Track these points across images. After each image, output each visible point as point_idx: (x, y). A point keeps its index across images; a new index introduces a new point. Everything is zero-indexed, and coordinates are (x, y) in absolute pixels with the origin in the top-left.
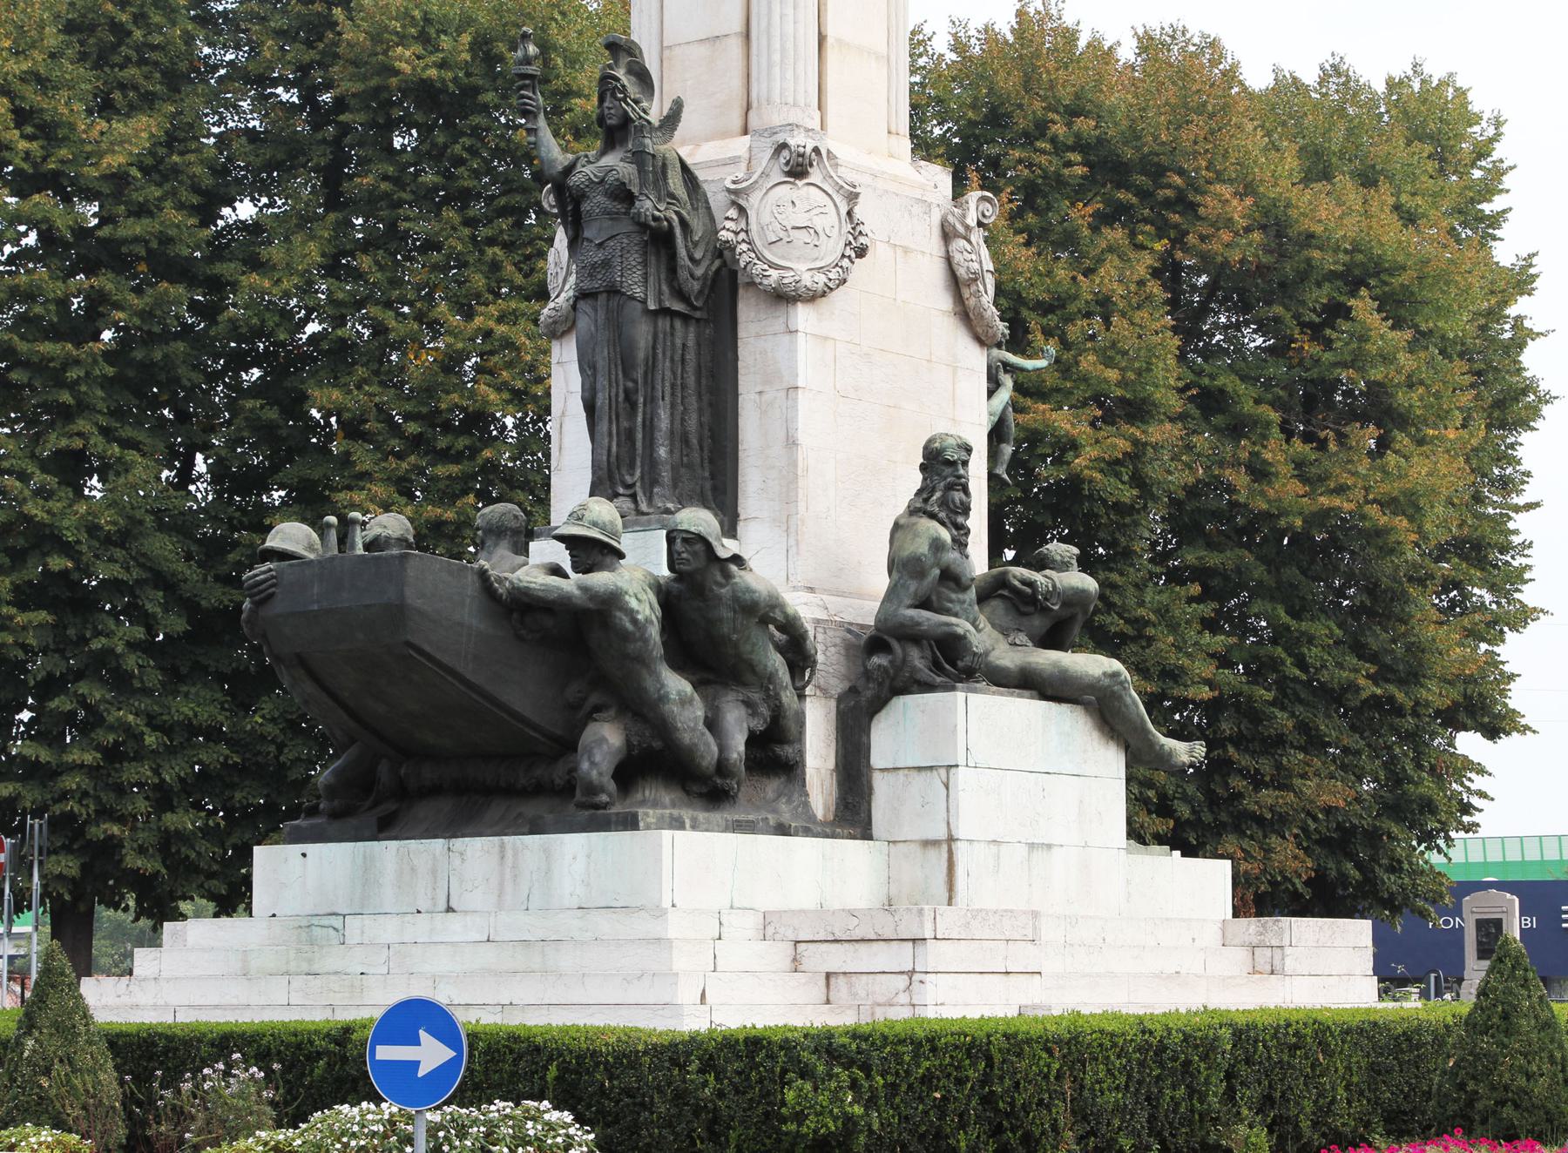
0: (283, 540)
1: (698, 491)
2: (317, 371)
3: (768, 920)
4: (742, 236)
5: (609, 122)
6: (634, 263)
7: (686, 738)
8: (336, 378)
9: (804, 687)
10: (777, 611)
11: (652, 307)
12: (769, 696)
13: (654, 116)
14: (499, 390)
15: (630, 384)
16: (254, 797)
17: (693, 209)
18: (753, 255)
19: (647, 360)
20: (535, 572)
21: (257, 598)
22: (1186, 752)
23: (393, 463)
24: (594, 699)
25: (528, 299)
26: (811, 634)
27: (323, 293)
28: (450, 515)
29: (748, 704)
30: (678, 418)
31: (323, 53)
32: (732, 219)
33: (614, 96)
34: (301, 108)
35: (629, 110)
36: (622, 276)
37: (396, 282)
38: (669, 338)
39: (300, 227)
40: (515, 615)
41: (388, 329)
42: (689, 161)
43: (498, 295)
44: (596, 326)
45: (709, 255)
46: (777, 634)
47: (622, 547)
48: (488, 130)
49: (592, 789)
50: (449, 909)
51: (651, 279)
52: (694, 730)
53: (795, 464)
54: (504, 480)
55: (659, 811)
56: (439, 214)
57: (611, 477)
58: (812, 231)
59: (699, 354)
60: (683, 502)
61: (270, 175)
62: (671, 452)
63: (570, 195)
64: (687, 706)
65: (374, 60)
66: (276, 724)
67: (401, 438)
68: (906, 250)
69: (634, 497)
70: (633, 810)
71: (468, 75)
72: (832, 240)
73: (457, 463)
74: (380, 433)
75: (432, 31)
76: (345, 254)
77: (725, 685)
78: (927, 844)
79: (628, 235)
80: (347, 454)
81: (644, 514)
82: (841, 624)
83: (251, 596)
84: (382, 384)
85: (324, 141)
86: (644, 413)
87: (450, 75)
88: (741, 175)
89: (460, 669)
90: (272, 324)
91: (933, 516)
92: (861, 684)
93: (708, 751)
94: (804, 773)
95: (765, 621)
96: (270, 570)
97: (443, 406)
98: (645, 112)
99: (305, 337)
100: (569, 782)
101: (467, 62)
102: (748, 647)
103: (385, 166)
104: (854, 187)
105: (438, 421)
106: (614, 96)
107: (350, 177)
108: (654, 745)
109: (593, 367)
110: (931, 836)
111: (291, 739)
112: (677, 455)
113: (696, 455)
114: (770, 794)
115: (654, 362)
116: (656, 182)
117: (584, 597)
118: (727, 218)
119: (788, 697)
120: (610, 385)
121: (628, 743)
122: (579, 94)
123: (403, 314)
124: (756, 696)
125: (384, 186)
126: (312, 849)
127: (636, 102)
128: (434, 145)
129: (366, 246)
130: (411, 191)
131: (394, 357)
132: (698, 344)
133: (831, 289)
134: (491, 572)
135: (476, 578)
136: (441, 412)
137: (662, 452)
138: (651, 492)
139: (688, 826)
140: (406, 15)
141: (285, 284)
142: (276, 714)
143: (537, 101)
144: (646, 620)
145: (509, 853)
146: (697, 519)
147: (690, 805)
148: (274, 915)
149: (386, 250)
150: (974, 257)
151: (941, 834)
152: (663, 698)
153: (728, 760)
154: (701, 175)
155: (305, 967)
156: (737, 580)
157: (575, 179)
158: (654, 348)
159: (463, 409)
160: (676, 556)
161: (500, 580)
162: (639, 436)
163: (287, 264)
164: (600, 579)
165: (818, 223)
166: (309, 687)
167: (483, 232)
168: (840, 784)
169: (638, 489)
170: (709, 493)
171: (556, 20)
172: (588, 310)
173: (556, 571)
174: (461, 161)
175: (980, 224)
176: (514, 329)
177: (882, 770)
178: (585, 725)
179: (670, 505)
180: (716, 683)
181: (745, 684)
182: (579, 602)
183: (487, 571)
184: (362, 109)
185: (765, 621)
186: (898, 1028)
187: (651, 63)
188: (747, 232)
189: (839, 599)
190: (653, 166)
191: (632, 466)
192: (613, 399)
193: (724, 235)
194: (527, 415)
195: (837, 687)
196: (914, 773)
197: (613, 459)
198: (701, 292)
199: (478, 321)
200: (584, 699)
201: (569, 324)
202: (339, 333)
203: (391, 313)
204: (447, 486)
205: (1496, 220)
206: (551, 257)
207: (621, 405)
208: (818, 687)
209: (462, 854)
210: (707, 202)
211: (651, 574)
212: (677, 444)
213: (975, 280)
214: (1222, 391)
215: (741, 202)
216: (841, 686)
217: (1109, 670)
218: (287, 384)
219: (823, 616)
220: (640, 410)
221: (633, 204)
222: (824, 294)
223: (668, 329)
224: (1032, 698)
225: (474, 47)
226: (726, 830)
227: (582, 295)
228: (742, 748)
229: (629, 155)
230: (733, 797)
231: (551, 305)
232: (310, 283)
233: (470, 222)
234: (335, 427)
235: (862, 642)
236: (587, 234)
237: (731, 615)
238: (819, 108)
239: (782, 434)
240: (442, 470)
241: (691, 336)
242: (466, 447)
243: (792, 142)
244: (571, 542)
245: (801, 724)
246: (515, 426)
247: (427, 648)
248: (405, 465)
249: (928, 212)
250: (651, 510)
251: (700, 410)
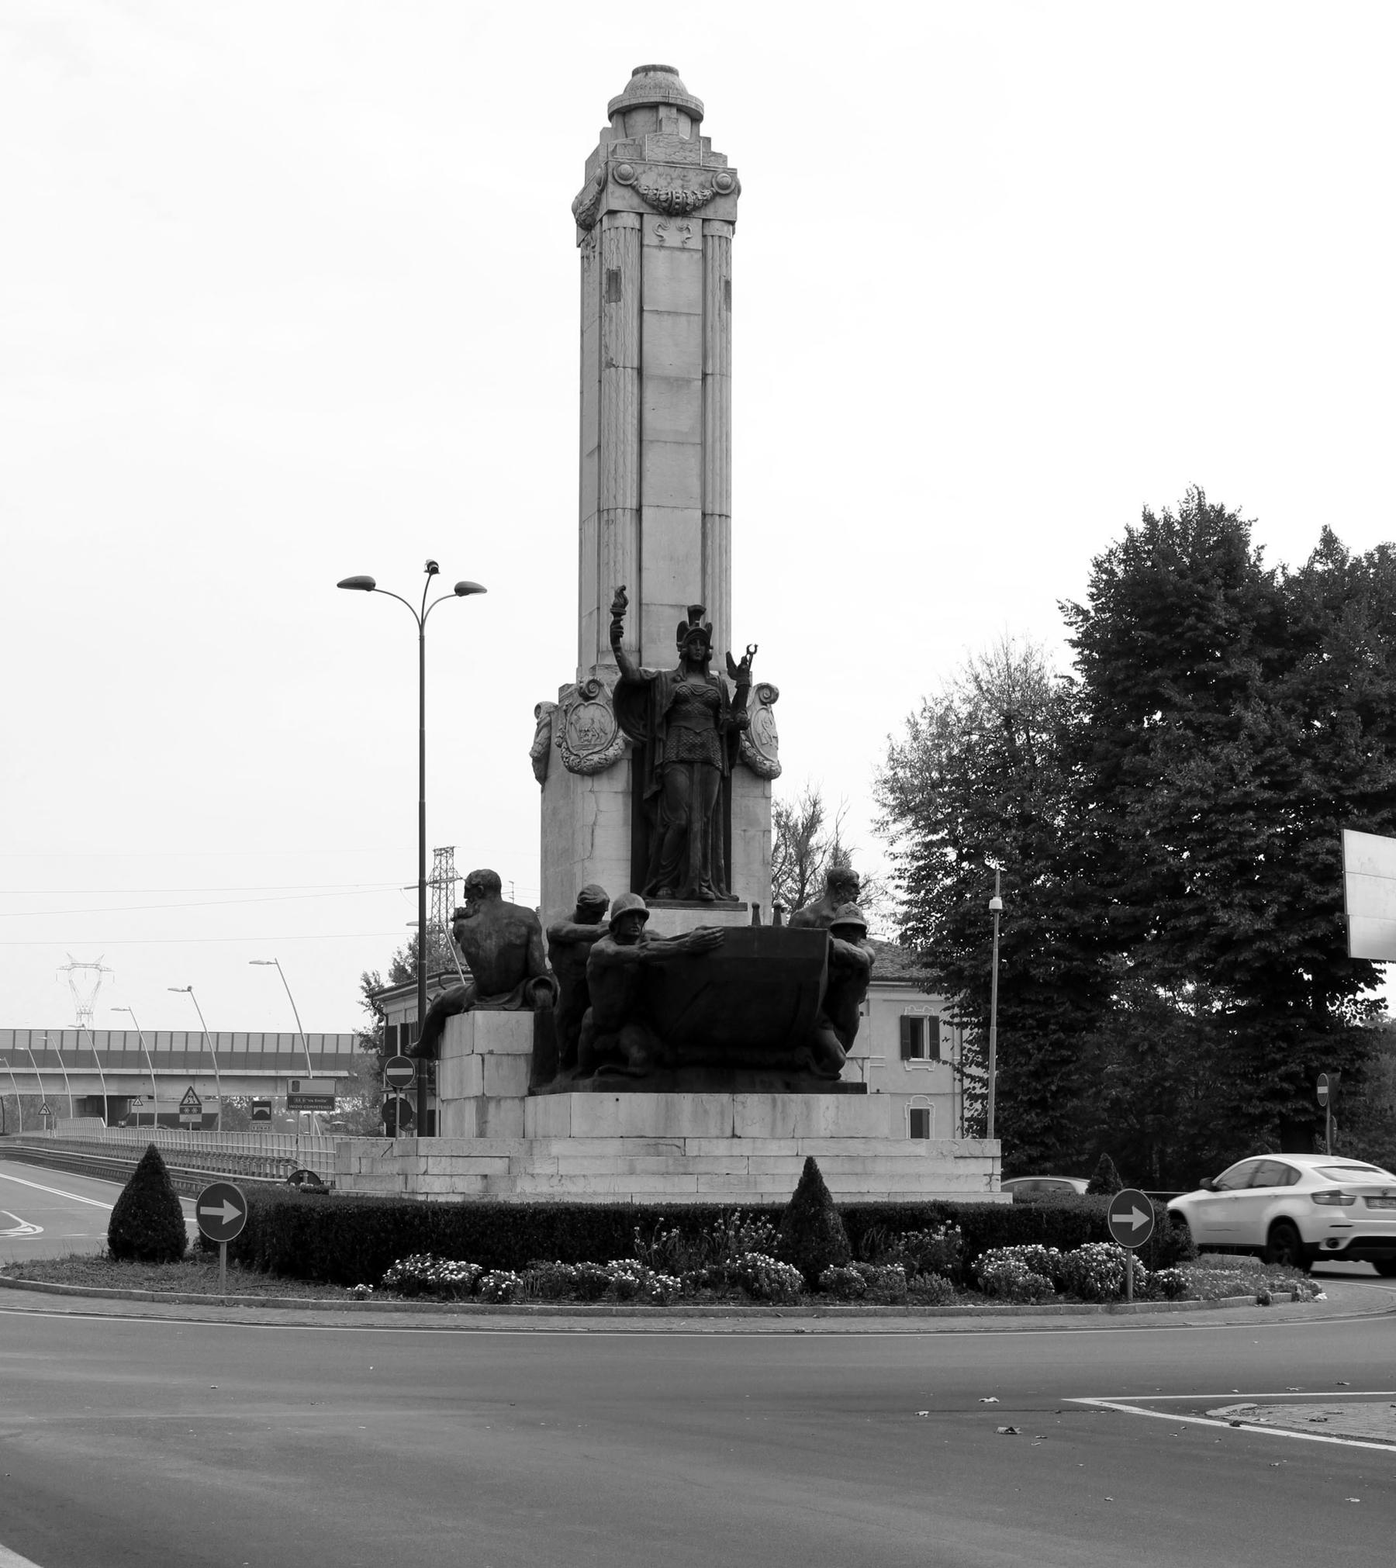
50: (734, 1136)
145: (779, 1104)
155: (681, 1170)
209: (743, 1103)
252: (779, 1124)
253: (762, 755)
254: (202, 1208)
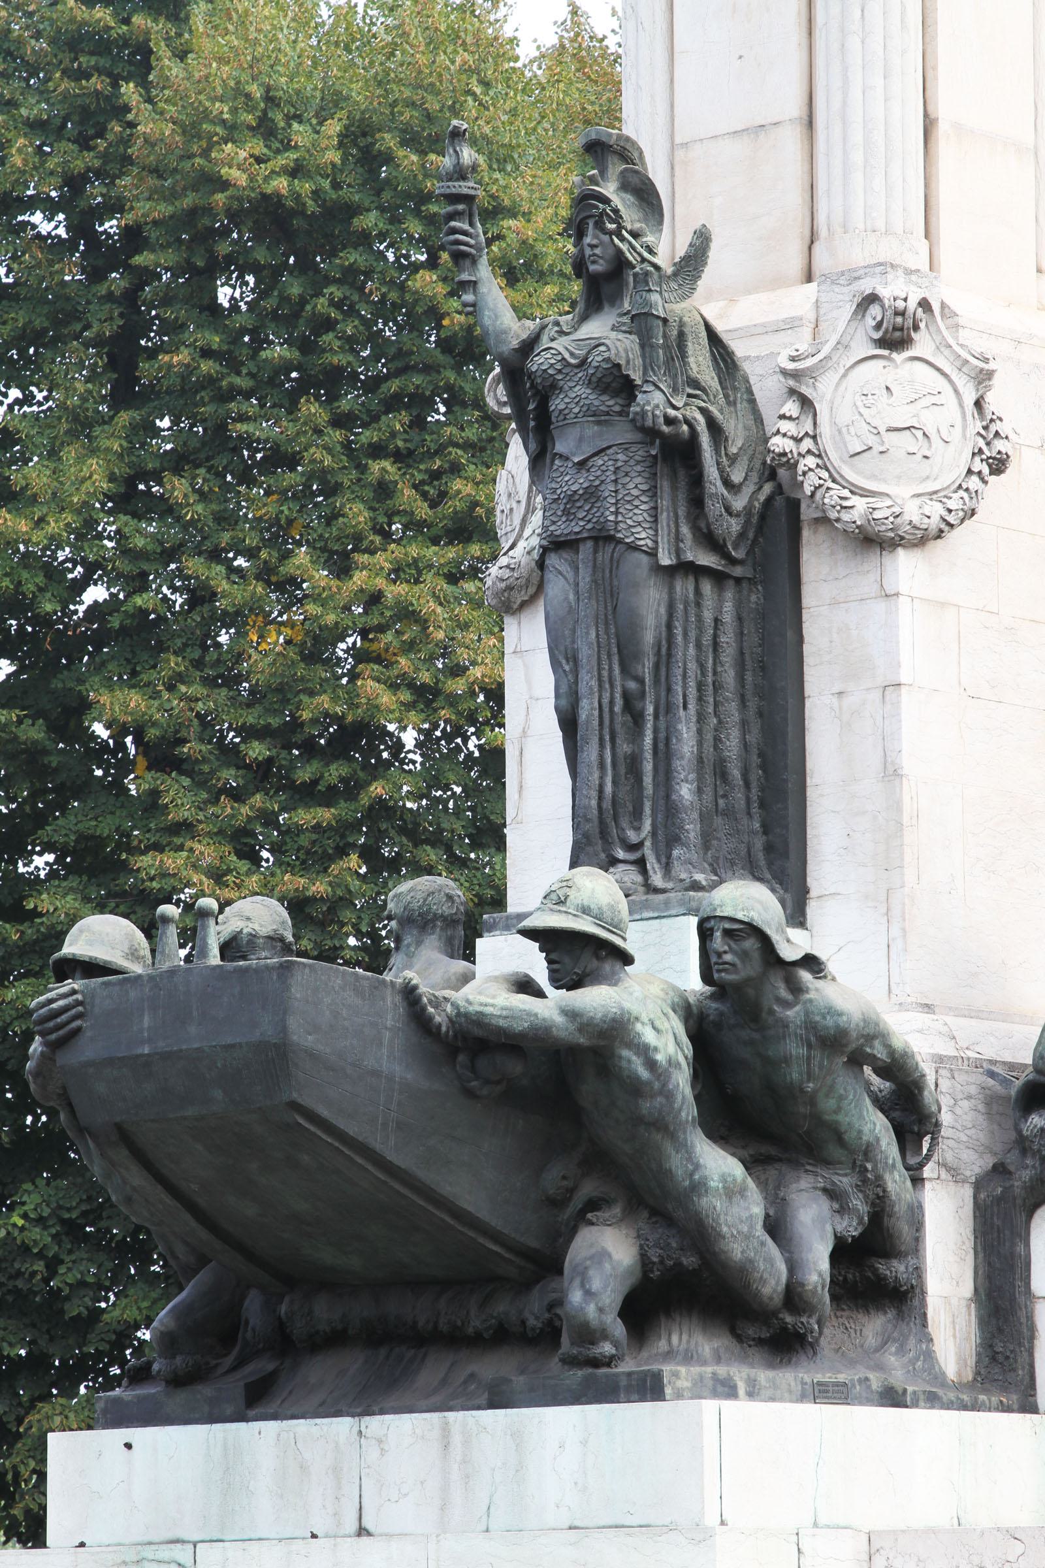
0: (90, 943)
1: (743, 853)
2: (103, 664)
3: (876, 1545)
4: (807, 444)
5: (592, 268)
6: (635, 492)
7: (736, 1251)
8: (134, 673)
9: (921, 1166)
10: (877, 1043)
11: (665, 560)
12: (865, 1181)
13: (664, 259)
14: (393, 687)
15: (632, 685)
16: (11, 1345)
17: (729, 403)
18: (825, 475)
20: (493, 988)
21: (53, 1037)
23: (226, 807)
24: (589, 1189)
25: (435, 541)
26: (930, 1079)
27: (110, 539)
28: (320, 888)
29: (832, 1194)
30: (709, 737)
31: (105, 156)
32: (790, 418)
33: (600, 226)
34: (71, 245)
35: (624, 247)
36: (617, 513)
37: (226, 520)
38: (692, 611)
39: (73, 434)
40: (461, 1058)
41: (214, 594)
42: (719, 327)
43: (387, 535)
44: (577, 593)
45: (754, 477)
46: (876, 1080)
47: (629, 947)
48: (368, 274)
49: (588, 1335)
50: (362, 1531)
51: (663, 517)
52: (748, 1237)
53: (898, 807)
54: (402, 831)
55: (696, 1370)
56: (292, 409)
57: (604, 833)
58: (919, 434)
60: (721, 870)
61: (22, 352)
62: (700, 791)
63: (533, 386)
64: (738, 1197)
65: (187, 165)
66: (45, 1228)
67: (238, 768)
69: (641, 863)
70: (655, 1367)
71: (336, 186)
72: (951, 447)
73: (328, 806)
74: (205, 760)
75: (278, 118)
76: (145, 476)
77: (795, 1164)
79: (625, 447)
80: (155, 794)
81: (656, 891)
82: (977, 1064)
83: (42, 1034)
84: (210, 682)
85: (110, 297)
86: (656, 731)
87: (307, 187)
88: (803, 347)
89: (378, 1146)
90: (32, 587)
92: (1012, 1159)
94: (923, 1303)
95: (857, 1060)
96: (74, 992)
97: (306, 715)
98: (650, 251)
99: (81, 609)
100: (550, 1322)
101: (333, 165)
102: (832, 1103)
103: (207, 335)
104: (986, 361)
105: (298, 738)
106: (600, 226)
107: (152, 354)
108: (685, 1261)
109: (574, 659)
111: (70, 1252)
112: (708, 796)
113: (739, 795)
114: (871, 1340)
115: (669, 648)
116: (669, 360)
117: (572, 1027)
118: (783, 417)
119: (896, 1182)
120: (600, 686)
121: (644, 1258)
122: (512, 213)
123: (239, 571)
124: (845, 1181)
125: (207, 367)
126: (140, 1435)
127: (635, 235)
128: (284, 299)
129: (179, 462)
130: (250, 374)
131: (223, 638)
132: (740, 619)
133: (951, 526)
134: (423, 989)
135: (398, 999)
136: (302, 725)
137: (685, 792)
138: (669, 857)
139: (741, 1392)
140: (239, 93)
141: (53, 527)
142: (46, 1212)
143: (476, 237)
144: (670, 1061)
145: (457, 1439)
147: (744, 1359)
148: (82, 1545)
149: (209, 470)
152: (699, 1187)
153: (803, 1285)
154: (740, 348)
156: (812, 995)
157: (539, 362)
158: (670, 626)
159: (339, 719)
160: (714, 959)
161: (437, 1003)
162: (648, 767)
163: (54, 494)
165: (930, 420)
166: (137, 1178)
167: (367, 436)
168: (983, 1323)
169: (648, 851)
170: (761, 856)
171: (474, 94)
172: (564, 567)
173: (525, 986)
174: (328, 325)
176: (416, 589)
178: (573, 1232)
179: (700, 877)
180: (780, 1160)
181: (827, 1163)
182: (563, 1034)
183: (415, 988)
184: (169, 245)
185: (857, 1060)
187: (657, 172)
188: (814, 437)
189: (973, 1022)
190: (665, 336)
191: (637, 814)
192: (606, 710)
193: (779, 444)
194: (435, 726)
195: (975, 1164)
197: (607, 804)
198: (742, 535)
199: (359, 578)
200: (572, 1191)
201: (532, 590)
202: (138, 601)
203: (220, 569)
204: (314, 842)
206: (501, 486)
207: (619, 719)
208: (942, 1164)
209: (380, 1441)
210: (750, 391)
211: (675, 988)
212: (709, 779)
215: (804, 390)
216: (980, 1162)
218: (56, 684)
219: (948, 1050)
220: (649, 725)
221: (632, 398)
222: (940, 535)
223: (691, 596)
225: (346, 139)
226: (802, 1398)
227: (554, 545)
228: (825, 1265)
229: (626, 319)
230: (812, 1345)
231: (503, 561)
232: (91, 523)
233: (341, 421)
234: (132, 750)
235: (1013, 1092)
236: (560, 447)
237: (803, 1051)
238: (927, 237)
240: (305, 817)
241: (728, 606)
242: (342, 780)
243: (885, 293)
244: (548, 939)
245: (918, 1225)
246: (419, 745)
247: (324, 1112)
248: (245, 810)
250: (670, 885)
251: (744, 724)
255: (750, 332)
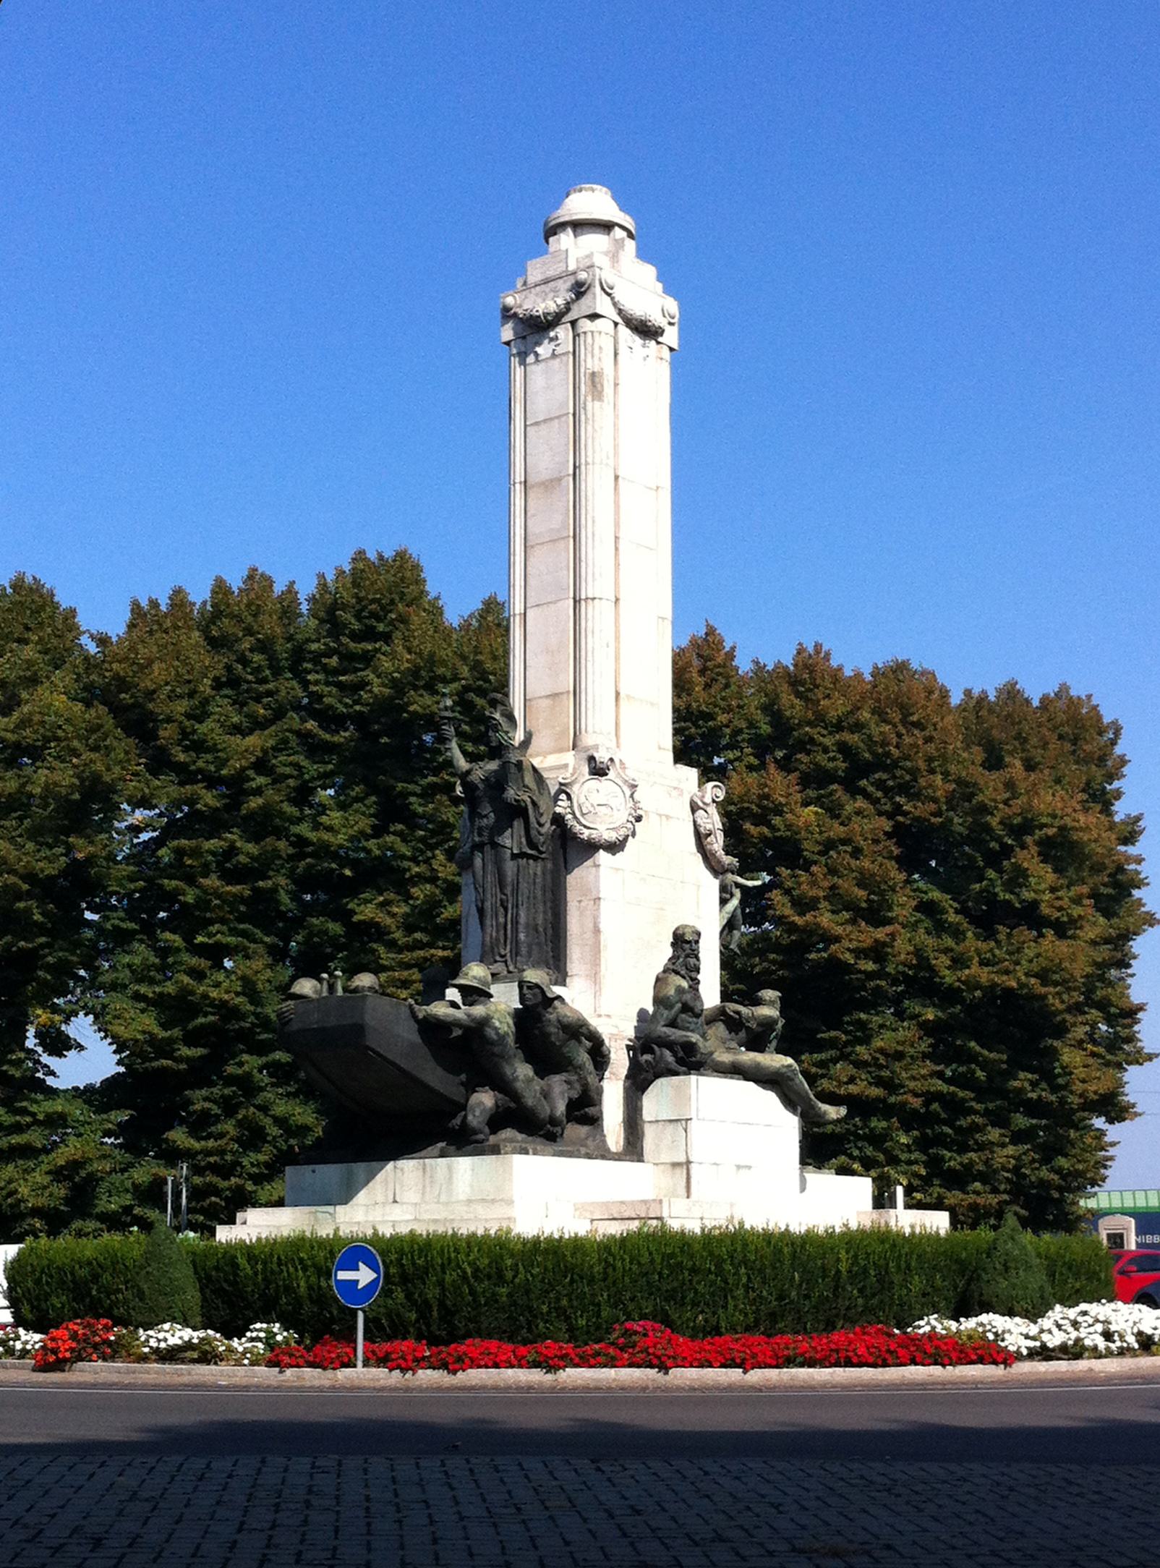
19: (513, 880)
22: (834, 1112)
42: (536, 765)
50: (395, 1202)
59: (544, 879)
62: (527, 936)
68: (668, 817)
69: (506, 962)
78: (675, 1165)
91: (677, 973)
93: (545, 1111)
110: (676, 1160)
119: (592, 1079)
121: (497, 1105)
132: (544, 873)
137: (522, 936)
146: (533, 975)
147: (533, 1142)
150: (709, 821)
151: (683, 1159)
154: (545, 775)
158: (518, 875)
164: (478, 1010)
165: (613, 803)
169: (508, 957)
175: (714, 801)
177: (649, 1122)
186: (1049, 1377)
196: (668, 1124)
205: (1118, 795)
213: (710, 835)
214: (932, 901)
217: (786, 1064)
219: (615, 1031)
224: (738, 1079)
226: (554, 1155)
239: (591, 925)
241: (539, 869)
249: (681, 795)
251: (545, 912)
252: (428, 1189)
253: (589, 828)
254: (339, 1273)
255: (551, 769)
